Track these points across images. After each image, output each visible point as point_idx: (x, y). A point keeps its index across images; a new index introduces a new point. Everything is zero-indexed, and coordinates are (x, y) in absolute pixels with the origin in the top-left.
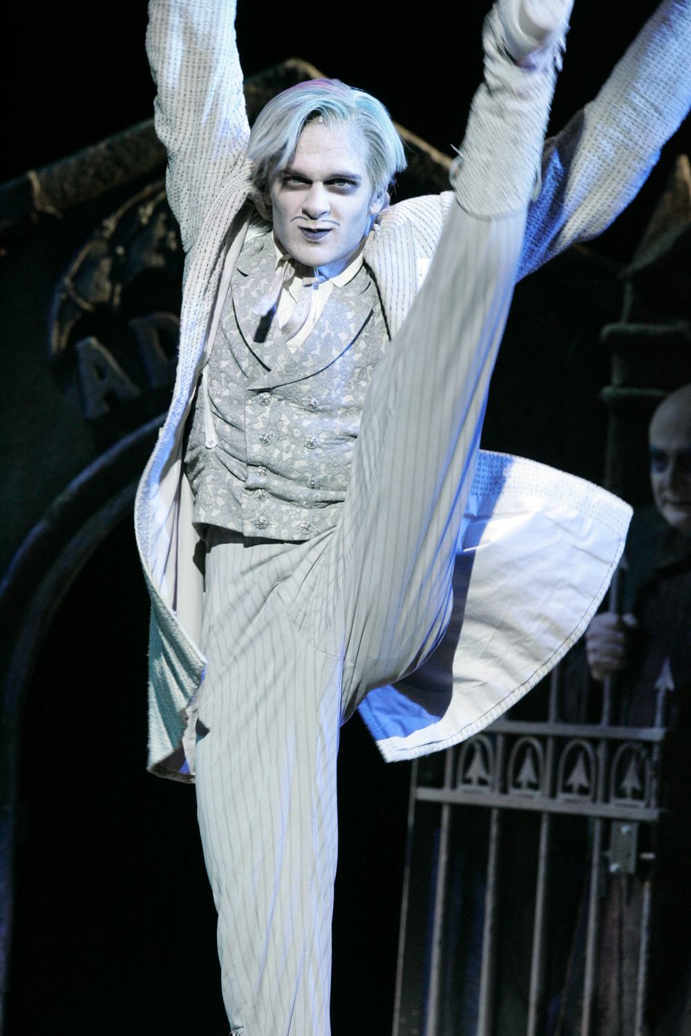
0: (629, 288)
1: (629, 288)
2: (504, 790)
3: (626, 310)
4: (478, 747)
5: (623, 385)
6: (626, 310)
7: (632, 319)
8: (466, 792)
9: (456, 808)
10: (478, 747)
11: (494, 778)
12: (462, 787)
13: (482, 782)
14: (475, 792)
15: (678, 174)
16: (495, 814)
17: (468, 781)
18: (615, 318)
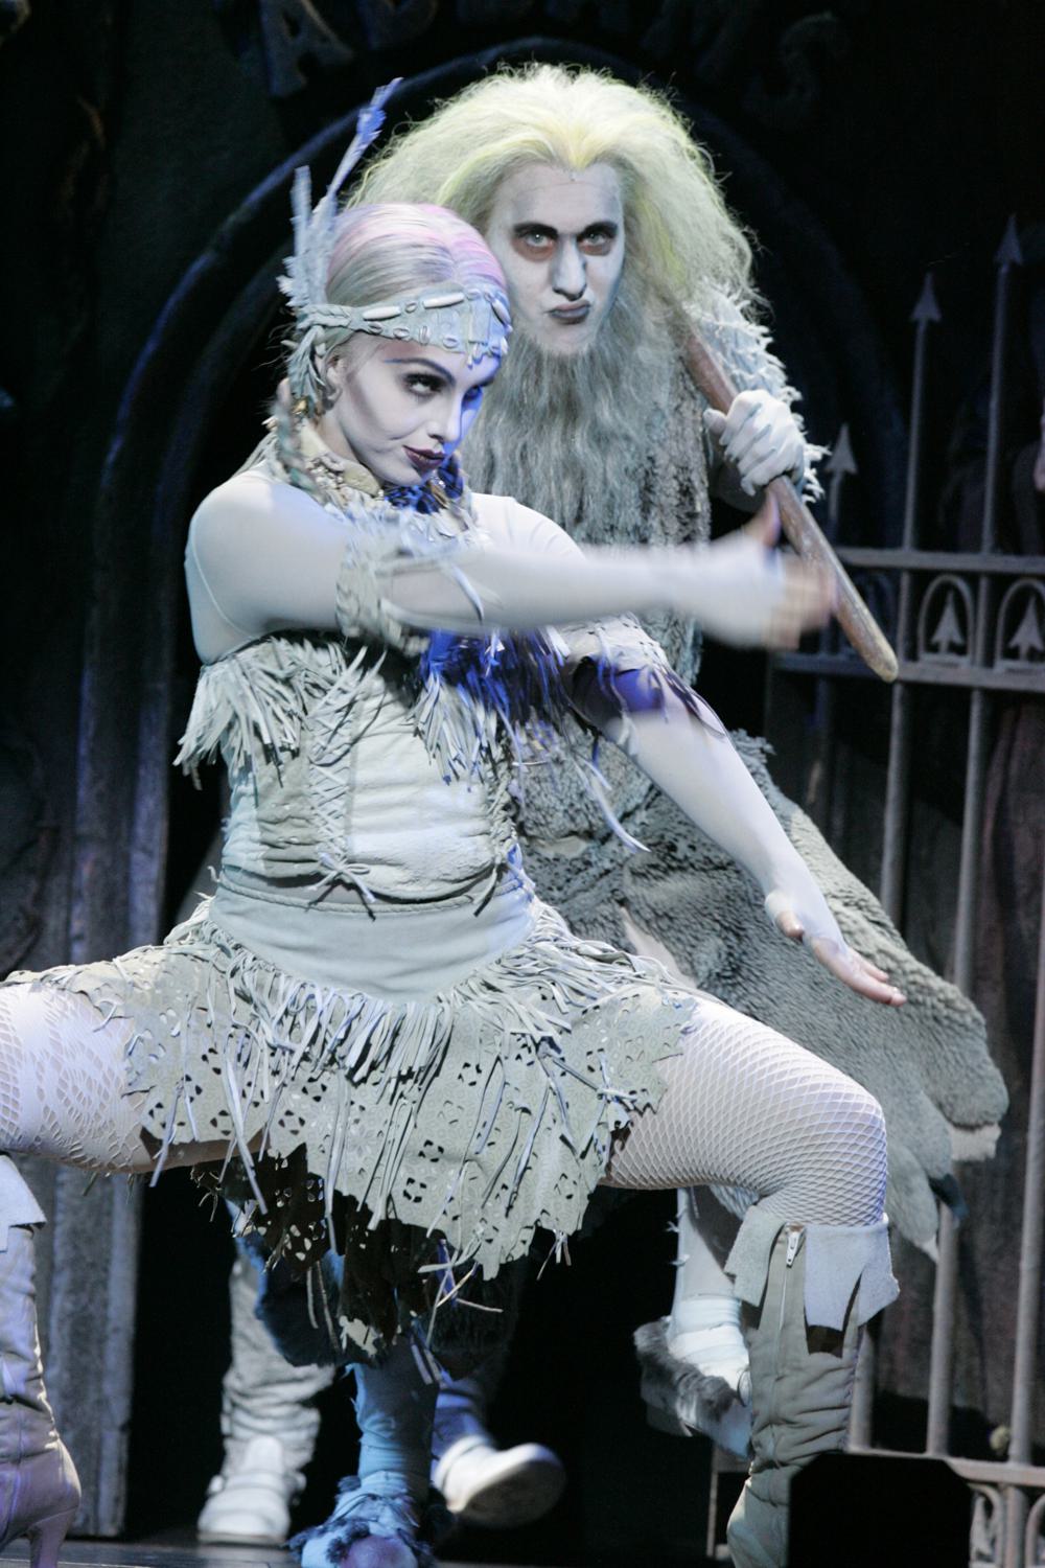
2: (989, 662)
13: (959, 650)
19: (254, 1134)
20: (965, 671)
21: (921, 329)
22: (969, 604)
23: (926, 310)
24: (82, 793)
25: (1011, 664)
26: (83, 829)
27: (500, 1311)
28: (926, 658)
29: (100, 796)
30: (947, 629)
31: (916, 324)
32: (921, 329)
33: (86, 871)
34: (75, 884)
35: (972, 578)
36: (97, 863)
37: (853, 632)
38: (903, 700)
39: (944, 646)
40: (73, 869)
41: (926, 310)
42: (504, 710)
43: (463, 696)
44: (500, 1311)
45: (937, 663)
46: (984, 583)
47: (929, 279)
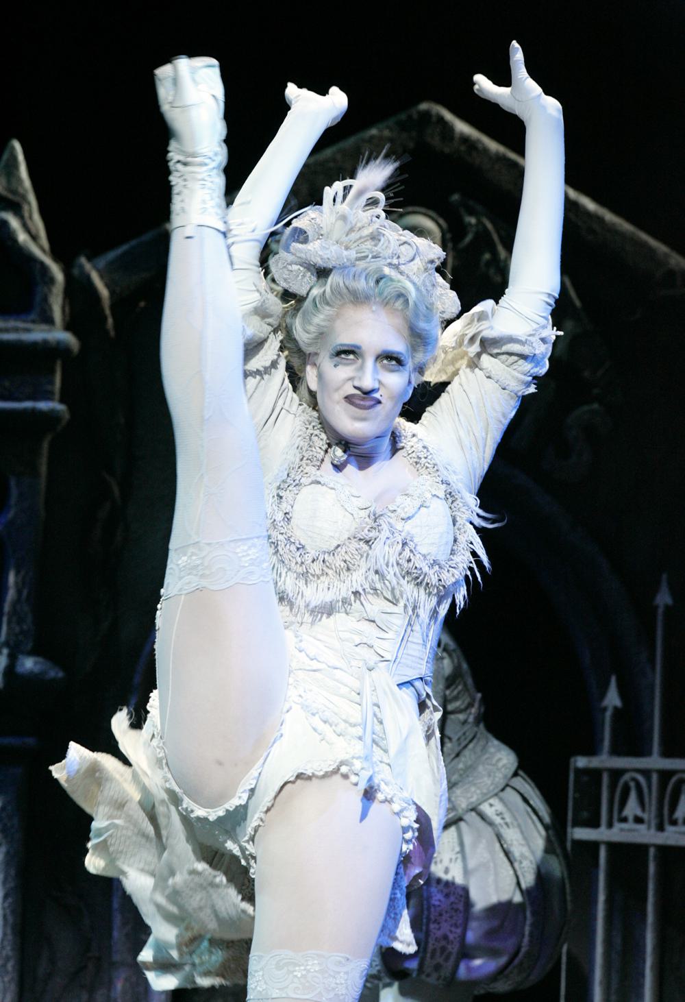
2: (660, 828)
4: (632, 784)
8: (622, 830)
9: (613, 847)
10: (632, 784)
11: (650, 815)
12: (618, 826)
13: (638, 820)
14: (630, 830)
16: (652, 851)
17: (624, 820)
19: (364, 821)
20: (645, 835)
21: (660, 611)
22: (646, 790)
23: (664, 598)
24: (116, 934)
25: (624, 825)
26: (117, 957)
27: (402, 199)
28: (670, 829)
29: (127, 935)
30: (632, 808)
31: (657, 607)
32: (660, 611)
33: (119, 986)
34: (112, 994)
35: (646, 773)
36: (126, 980)
37: (487, 816)
38: (655, 857)
39: (631, 818)
40: (110, 984)
41: (664, 598)
42: (28, 330)
43: (287, 374)
44: (402, 199)
45: (676, 832)
46: (655, 777)
47: (664, 576)
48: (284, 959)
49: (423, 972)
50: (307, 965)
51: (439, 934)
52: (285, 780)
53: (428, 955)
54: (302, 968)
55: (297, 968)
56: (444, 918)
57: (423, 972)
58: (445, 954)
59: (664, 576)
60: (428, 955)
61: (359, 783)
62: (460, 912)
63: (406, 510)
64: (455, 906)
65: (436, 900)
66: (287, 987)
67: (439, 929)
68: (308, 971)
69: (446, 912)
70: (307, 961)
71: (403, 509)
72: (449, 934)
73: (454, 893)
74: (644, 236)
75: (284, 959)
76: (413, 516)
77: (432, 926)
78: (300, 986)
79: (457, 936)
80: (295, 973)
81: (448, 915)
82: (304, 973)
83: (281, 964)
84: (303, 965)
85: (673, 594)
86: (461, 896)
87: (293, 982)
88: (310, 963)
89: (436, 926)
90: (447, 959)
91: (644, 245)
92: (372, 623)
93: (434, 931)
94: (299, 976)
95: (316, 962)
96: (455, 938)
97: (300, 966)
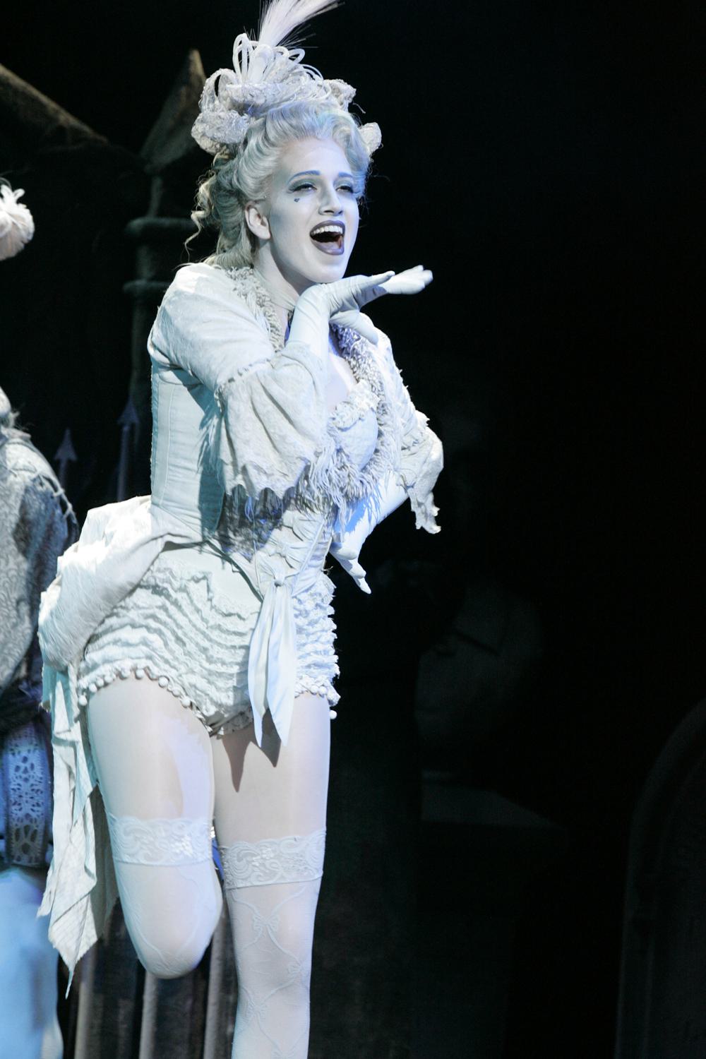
0: (157, 183)
1: (157, 183)
3: (155, 203)
5: (152, 279)
6: (155, 203)
7: (161, 213)
15: (192, 69)
18: (142, 213)
47: (68, 433)
48: (242, 850)
49: (13, 857)
50: (263, 854)
51: (21, 814)
52: (150, 681)
53: (13, 837)
54: (259, 857)
55: (254, 858)
56: (24, 799)
57: (13, 857)
58: (30, 834)
59: (68, 433)
60: (13, 837)
61: (127, 680)
62: (42, 792)
63: (344, 419)
64: (36, 788)
65: (15, 785)
66: (249, 877)
67: (20, 809)
68: (265, 859)
69: (26, 794)
70: (261, 850)
71: (342, 418)
72: (31, 813)
73: (33, 777)
74: (35, 92)
75: (242, 850)
76: (349, 428)
77: (13, 808)
78: (262, 874)
79: (39, 813)
80: (253, 863)
81: (29, 796)
82: (261, 861)
83: (241, 856)
84: (259, 855)
85: (77, 449)
86: (41, 778)
87: (254, 871)
88: (264, 852)
89: (17, 807)
90: (33, 839)
91: (35, 100)
92: (289, 529)
93: (15, 812)
94: (257, 865)
95: (269, 849)
96: (38, 816)
97: (255, 856)
